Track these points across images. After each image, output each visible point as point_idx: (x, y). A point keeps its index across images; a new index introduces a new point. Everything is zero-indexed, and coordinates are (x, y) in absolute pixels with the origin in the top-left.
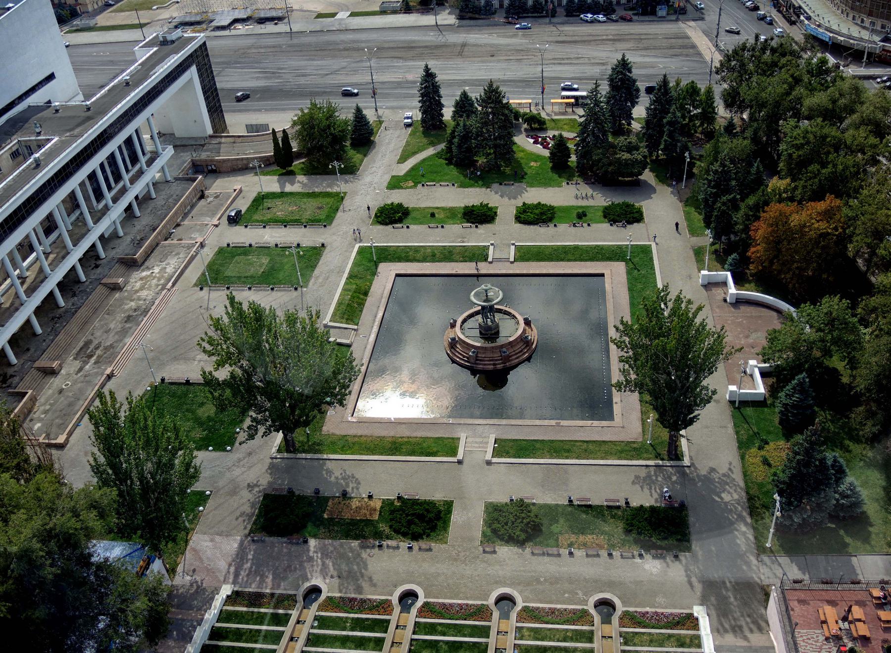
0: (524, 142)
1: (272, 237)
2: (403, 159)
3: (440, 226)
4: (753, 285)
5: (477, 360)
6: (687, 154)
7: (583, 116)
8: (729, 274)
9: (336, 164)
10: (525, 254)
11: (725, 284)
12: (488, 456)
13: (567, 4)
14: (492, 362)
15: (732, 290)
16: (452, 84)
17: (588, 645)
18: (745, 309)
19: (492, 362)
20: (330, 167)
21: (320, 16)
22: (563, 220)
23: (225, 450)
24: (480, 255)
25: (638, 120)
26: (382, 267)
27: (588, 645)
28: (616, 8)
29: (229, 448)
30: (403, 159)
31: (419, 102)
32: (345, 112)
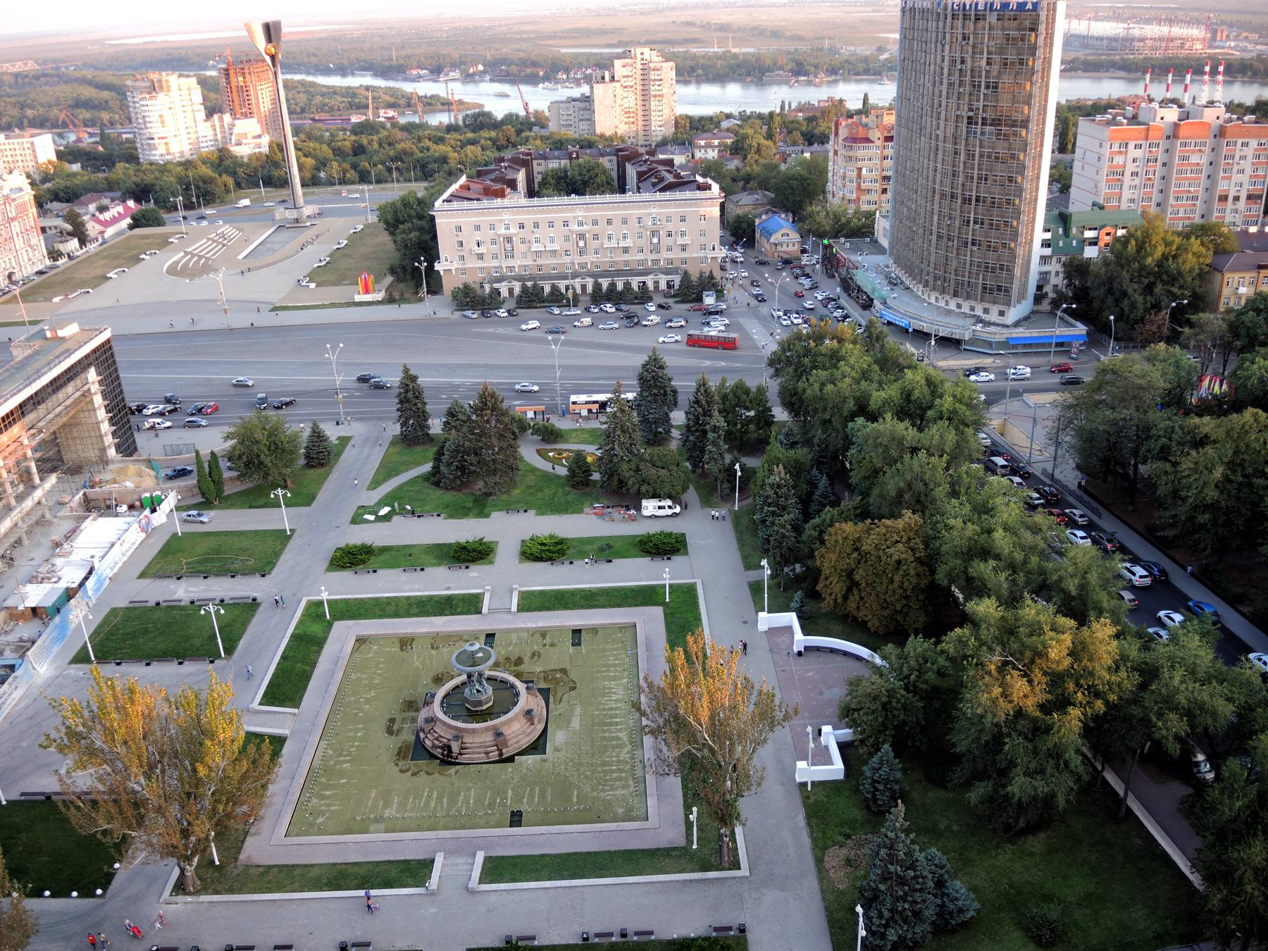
0: (528, 452)
1: (187, 591)
2: (375, 484)
3: (419, 568)
4: (1197, 843)
5: (462, 748)
6: (737, 467)
7: (605, 423)
8: (793, 615)
9: (280, 492)
10: (532, 602)
11: (789, 629)
12: (474, 882)
13: (593, 290)
14: (482, 750)
15: (800, 639)
16: (439, 389)
17: (289, 77)
18: (812, 657)
19: (482, 750)
20: (272, 496)
21: (275, 309)
22: (582, 555)
23: (94, 895)
24: (471, 604)
25: (677, 427)
26: (339, 626)
27: (289, 77)
28: (652, 295)
29: (99, 892)
30: (375, 484)
31: (398, 410)
32: (298, 428)
